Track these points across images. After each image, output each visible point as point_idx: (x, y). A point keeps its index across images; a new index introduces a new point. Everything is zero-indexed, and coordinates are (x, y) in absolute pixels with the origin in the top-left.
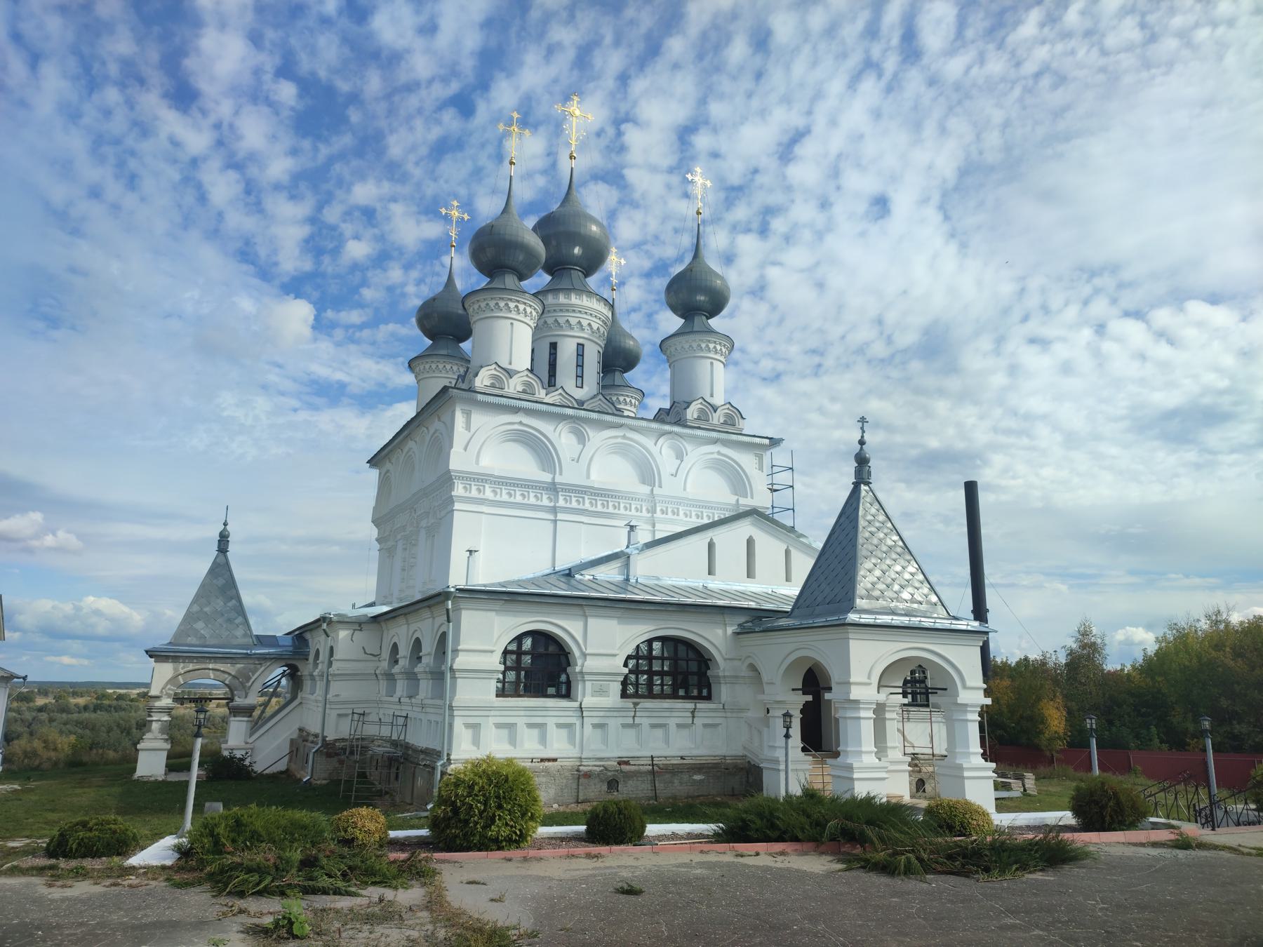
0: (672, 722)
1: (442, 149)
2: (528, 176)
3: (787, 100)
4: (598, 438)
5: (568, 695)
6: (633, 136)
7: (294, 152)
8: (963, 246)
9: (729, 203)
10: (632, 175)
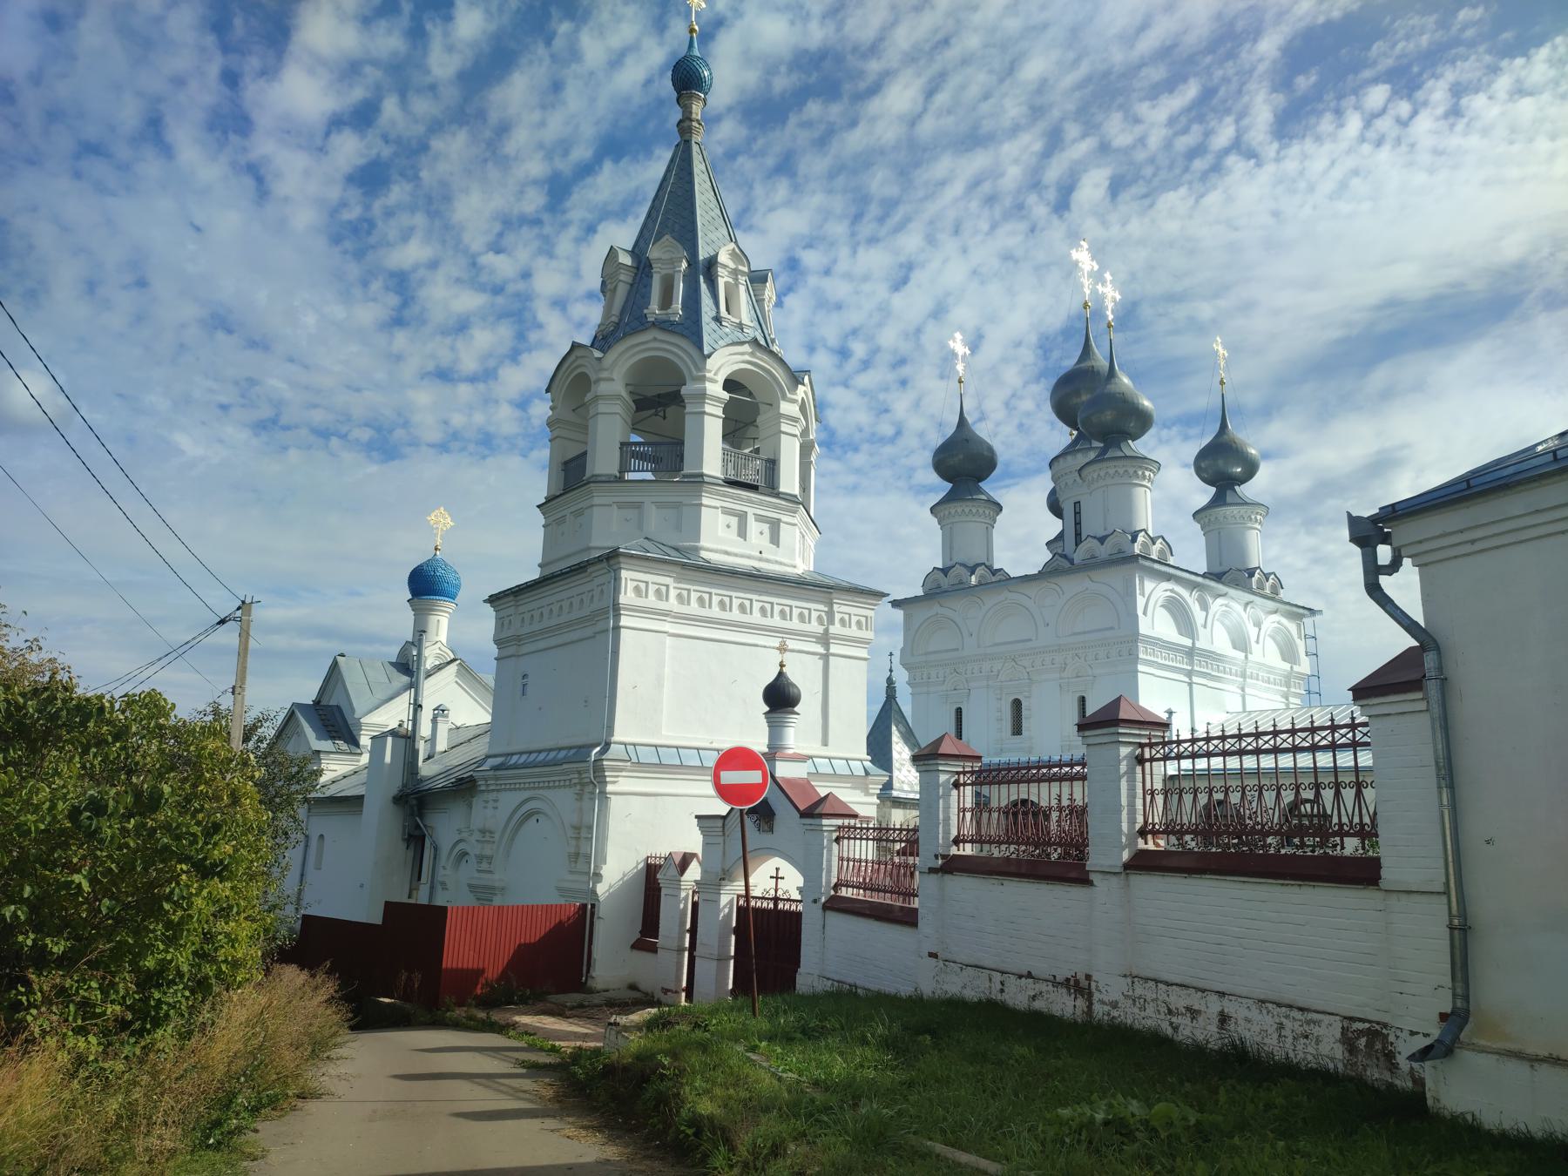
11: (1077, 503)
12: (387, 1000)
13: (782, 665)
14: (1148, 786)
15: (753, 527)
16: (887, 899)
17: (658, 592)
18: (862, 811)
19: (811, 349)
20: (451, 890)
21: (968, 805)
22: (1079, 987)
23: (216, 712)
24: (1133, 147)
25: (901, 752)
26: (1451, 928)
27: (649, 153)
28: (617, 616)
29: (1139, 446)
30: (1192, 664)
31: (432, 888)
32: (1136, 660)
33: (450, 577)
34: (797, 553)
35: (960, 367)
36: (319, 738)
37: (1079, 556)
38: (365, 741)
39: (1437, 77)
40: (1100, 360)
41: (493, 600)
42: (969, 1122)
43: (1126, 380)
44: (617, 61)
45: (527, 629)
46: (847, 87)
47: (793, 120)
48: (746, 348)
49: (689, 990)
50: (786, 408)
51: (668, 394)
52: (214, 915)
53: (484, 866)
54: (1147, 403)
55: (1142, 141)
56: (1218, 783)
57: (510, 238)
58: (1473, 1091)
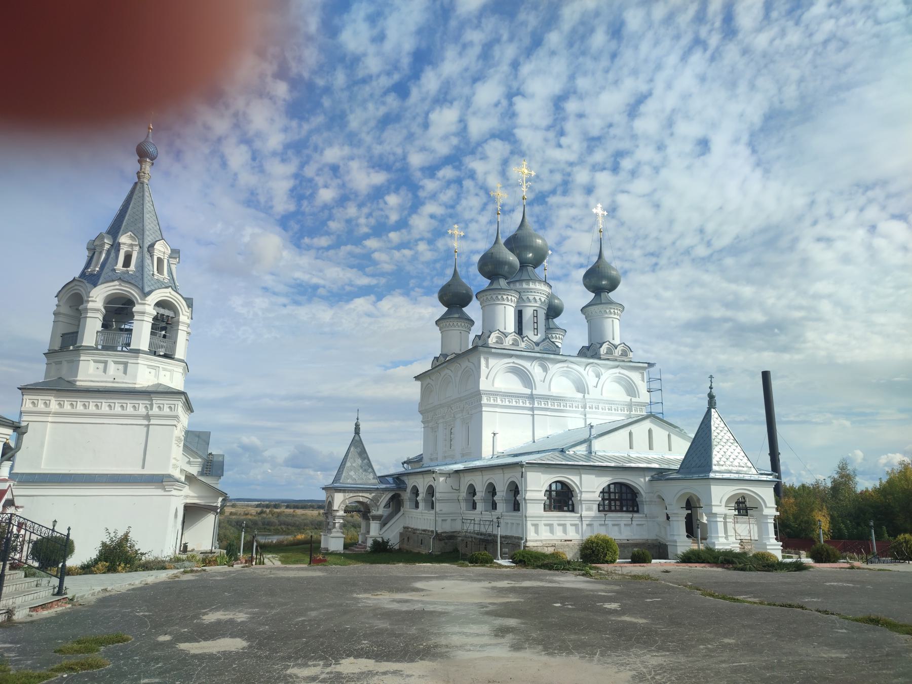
0: (622, 523)
1: (386, 121)
2: (445, 138)
3: (635, 72)
4: (554, 368)
5: (573, 511)
6: (521, 105)
7: (285, 130)
8: (767, 171)
9: (590, 150)
10: (520, 133)
48: (116, 283)
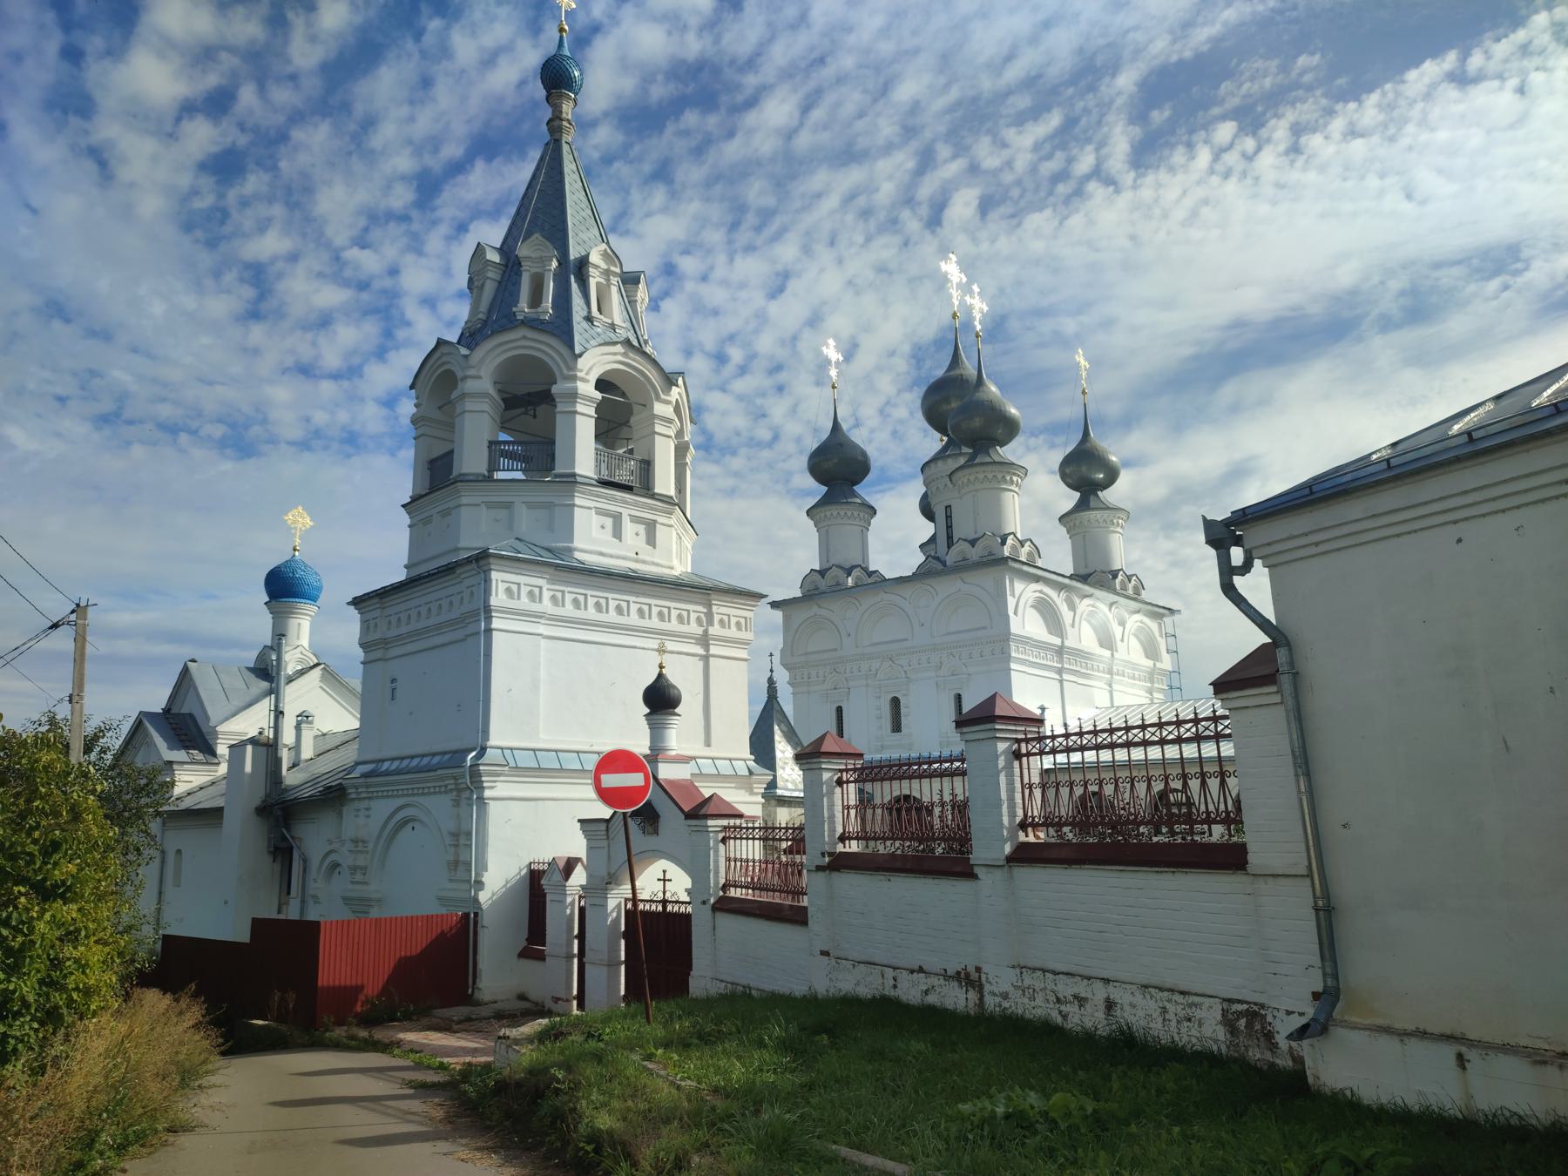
11: (948, 507)
12: (260, 1022)
13: (661, 667)
14: (1026, 780)
15: (629, 528)
16: (777, 899)
17: (531, 594)
18: (747, 810)
19: (688, 353)
20: (324, 904)
21: (852, 802)
22: (969, 979)
23: (52, 721)
24: (1001, 170)
25: (784, 751)
26: (1317, 910)
27: (523, 155)
28: (489, 618)
29: (1008, 452)
30: (1061, 661)
31: (303, 901)
32: (1008, 658)
33: (311, 579)
34: (675, 555)
35: (833, 373)
36: (171, 748)
37: (950, 559)
38: (222, 749)
39: (1278, 116)
40: (969, 368)
41: (357, 602)
42: (872, 1122)
43: (993, 388)
44: (490, 60)
45: (394, 632)
46: (724, 99)
47: (670, 128)
48: (619, 348)
49: (581, 998)
50: (659, 409)
51: (538, 393)
52: (61, 940)
53: (359, 877)
54: (1013, 411)
55: (1009, 164)
56: (1092, 776)
57: (376, 234)
58: (1349, 1067)
